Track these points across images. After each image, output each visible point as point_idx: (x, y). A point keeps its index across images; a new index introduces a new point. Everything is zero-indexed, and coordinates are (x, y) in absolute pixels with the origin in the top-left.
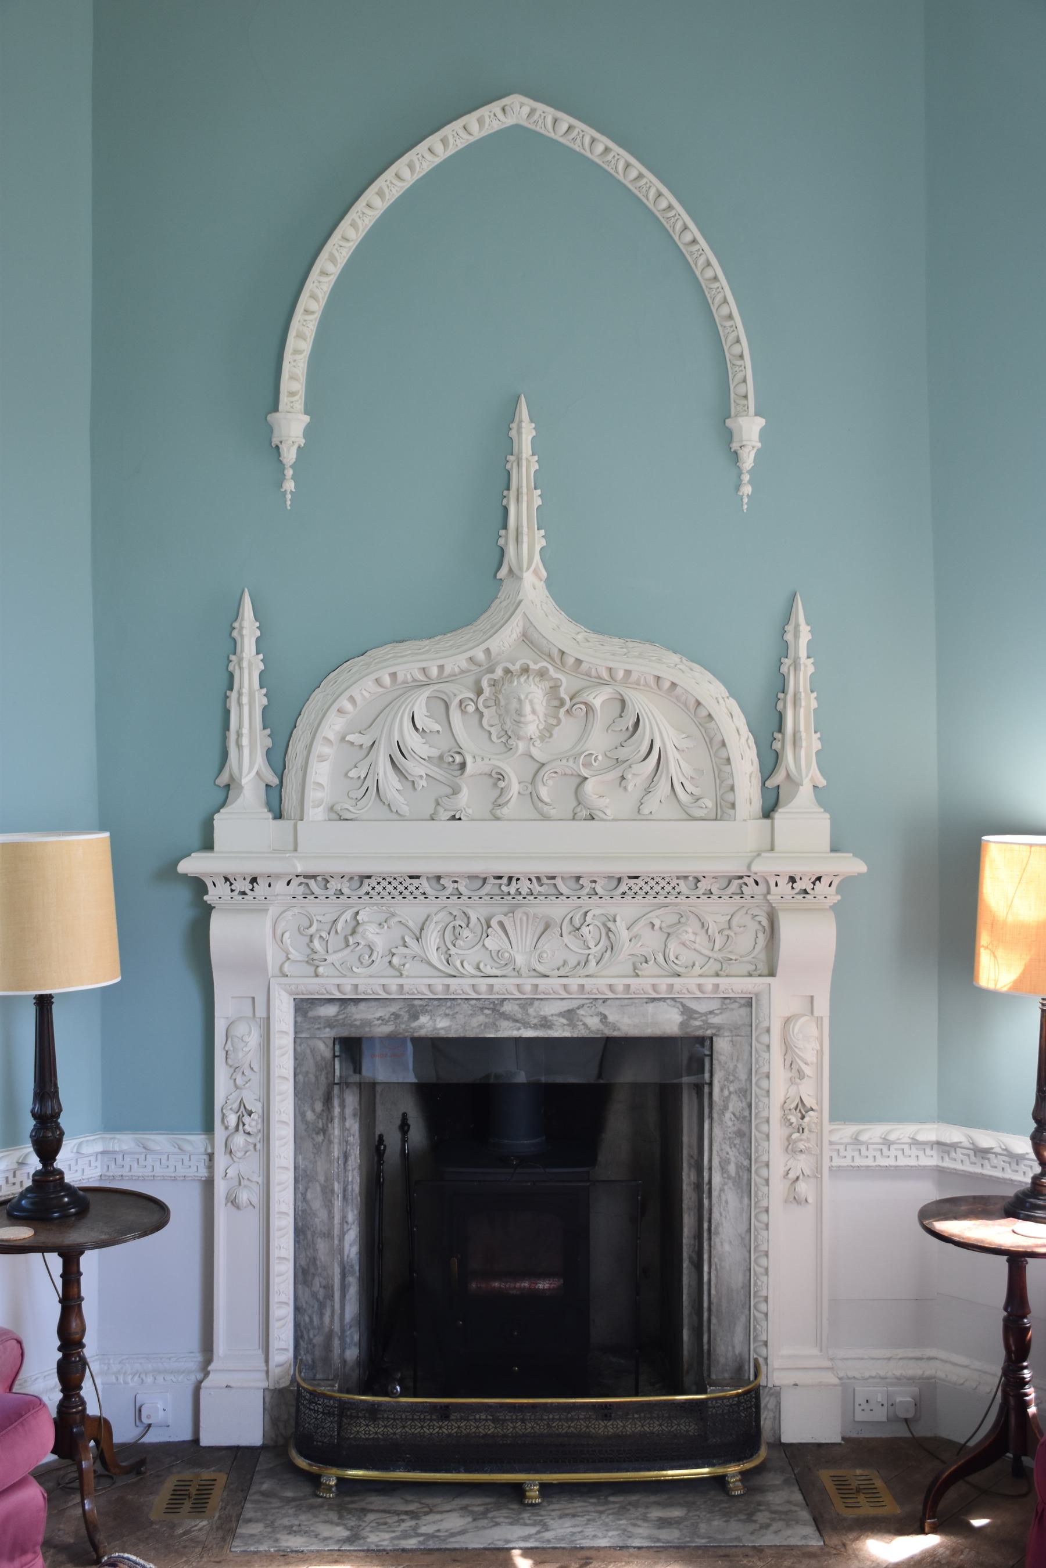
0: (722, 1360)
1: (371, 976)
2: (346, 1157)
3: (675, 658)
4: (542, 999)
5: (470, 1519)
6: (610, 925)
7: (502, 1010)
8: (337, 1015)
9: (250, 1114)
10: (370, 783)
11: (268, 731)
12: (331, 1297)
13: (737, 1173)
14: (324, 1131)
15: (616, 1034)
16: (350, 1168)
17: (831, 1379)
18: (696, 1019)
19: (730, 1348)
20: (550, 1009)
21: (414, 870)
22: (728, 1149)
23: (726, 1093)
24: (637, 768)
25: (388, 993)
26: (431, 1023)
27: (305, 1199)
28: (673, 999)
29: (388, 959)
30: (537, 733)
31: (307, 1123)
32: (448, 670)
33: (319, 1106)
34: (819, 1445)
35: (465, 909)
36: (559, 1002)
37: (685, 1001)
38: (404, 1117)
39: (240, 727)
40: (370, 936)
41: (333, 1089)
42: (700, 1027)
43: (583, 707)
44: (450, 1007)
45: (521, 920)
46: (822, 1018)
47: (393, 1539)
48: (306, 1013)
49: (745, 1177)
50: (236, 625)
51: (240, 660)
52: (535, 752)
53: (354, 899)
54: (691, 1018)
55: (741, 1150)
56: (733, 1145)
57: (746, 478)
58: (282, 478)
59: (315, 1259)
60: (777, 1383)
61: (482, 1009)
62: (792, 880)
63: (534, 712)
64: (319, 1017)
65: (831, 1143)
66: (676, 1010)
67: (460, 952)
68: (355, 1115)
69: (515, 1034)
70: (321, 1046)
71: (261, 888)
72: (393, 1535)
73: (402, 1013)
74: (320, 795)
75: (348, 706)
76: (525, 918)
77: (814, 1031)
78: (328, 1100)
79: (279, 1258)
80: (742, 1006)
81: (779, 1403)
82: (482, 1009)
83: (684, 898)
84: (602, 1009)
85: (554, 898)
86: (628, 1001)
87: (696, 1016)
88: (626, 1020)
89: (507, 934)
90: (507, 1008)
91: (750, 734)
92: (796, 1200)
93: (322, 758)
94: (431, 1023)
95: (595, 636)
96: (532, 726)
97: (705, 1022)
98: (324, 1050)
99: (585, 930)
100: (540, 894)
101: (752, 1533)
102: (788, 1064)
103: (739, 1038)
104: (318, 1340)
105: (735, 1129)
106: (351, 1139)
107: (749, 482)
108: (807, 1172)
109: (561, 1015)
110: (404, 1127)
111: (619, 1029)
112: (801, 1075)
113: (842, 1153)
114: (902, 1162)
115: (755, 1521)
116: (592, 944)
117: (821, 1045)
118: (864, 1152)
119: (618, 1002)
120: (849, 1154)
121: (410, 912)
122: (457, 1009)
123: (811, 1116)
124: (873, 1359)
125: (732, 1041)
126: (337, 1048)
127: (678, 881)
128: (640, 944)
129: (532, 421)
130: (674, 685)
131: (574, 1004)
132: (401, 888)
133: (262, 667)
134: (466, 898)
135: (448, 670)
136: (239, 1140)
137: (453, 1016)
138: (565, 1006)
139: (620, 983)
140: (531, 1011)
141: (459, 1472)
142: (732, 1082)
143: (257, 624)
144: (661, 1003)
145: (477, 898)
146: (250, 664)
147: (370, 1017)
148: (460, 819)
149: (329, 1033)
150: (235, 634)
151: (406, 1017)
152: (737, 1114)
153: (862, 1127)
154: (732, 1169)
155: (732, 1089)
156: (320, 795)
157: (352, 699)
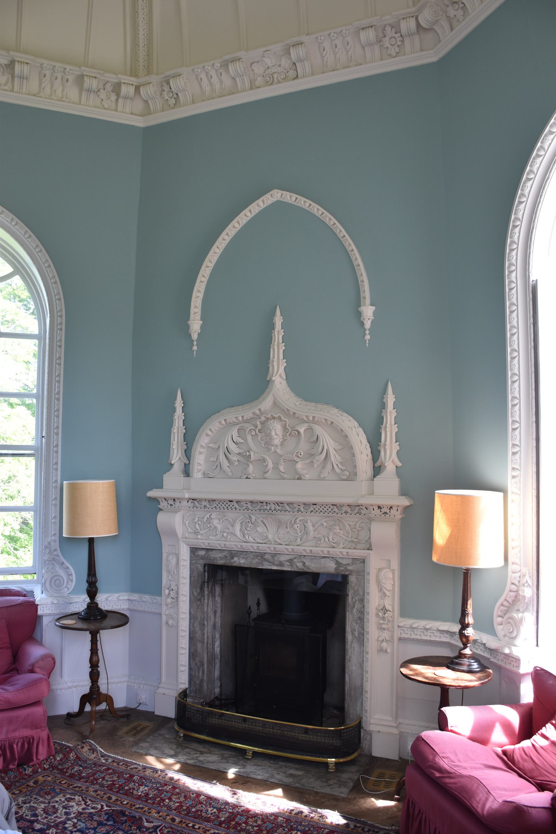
0: (352, 716)
1: (217, 540)
2: (215, 613)
3: (336, 411)
4: (280, 554)
5: (304, 772)
6: (305, 524)
7: (265, 557)
8: (205, 555)
9: (173, 590)
10: (218, 463)
11: (185, 443)
12: (203, 665)
13: (359, 636)
14: (200, 600)
15: (309, 571)
16: (217, 616)
17: (395, 731)
18: (342, 567)
19: (355, 712)
20: (283, 558)
21: (231, 498)
22: (355, 625)
23: (354, 600)
24: (317, 458)
25: (344, 556)
26: (238, 561)
27: (193, 627)
28: (332, 557)
29: (222, 534)
30: (279, 443)
31: (194, 596)
32: (245, 418)
33: (198, 590)
34: (388, 760)
35: (250, 515)
36: (286, 555)
37: (337, 559)
38: (258, 600)
39: (386, 440)
40: (215, 524)
41: (204, 584)
42: (343, 570)
43: (296, 432)
44: (245, 555)
45: (270, 521)
46: (394, 570)
47: (187, 759)
48: (194, 553)
49: (362, 638)
50: (385, 396)
51: (387, 412)
52: (279, 451)
53: (210, 509)
54: (339, 566)
55: (360, 625)
56: (357, 623)
57: (367, 332)
58: (365, 334)
59: (197, 650)
60: (371, 729)
61: (257, 556)
62: (379, 507)
63: (276, 434)
64: (199, 555)
65: (399, 626)
66: (333, 562)
67: (248, 532)
68: (219, 596)
69: (269, 567)
70: (200, 566)
71: (177, 503)
72: (188, 757)
73: (228, 555)
74: (200, 467)
75: (210, 433)
76: (271, 520)
77: (390, 575)
78: (202, 588)
79: (181, 648)
80: (361, 562)
81: (371, 739)
82: (257, 556)
83: (336, 514)
84: (303, 560)
85: (284, 512)
86: (314, 557)
87: (342, 565)
88: (313, 565)
89: (266, 526)
90: (267, 556)
91: (368, 444)
92: (381, 650)
93: (200, 453)
94: (238, 561)
95: (305, 402)
96: (277, 441)
97: (346, 568)
98: (201, 568)
99: (296, 526)
100: (279, 510)
101: (321, 787)
102: (379, 590)
103: (359, 576)
104: (198, 682)
105: (358, 616)
106: (218, 605)
107: (369, 334)
108: (387, 638)
109: (287, 561)
110: (258, 604)
111: (310, 569)
112: (385, 595)
113: (406, 632)
114: (433, 638)
115: (328, 782)
116: (299, 532)
117: (394, 582)
118: (416, 632)
119: (310, 557)
120: (409, 632)
121: (231, 515)
122: (248, 556)
123: (388, 614)
124: (419, 726)
125: (357, 577)
126: (206, 568)
127: (333, 507)
128: (317, 533)
129: (281, 315)
130: (332, 422)
131: (292, 557)
132: (227, 505)
133: (184, 418)
134: (263, 511)
135: (245, 418)
136: (169, 600)
137: (246, 559)
138: (288, 557)
139: (308, 549)
140: (276, 558)
141: (225, 740)
142: (357, 595)
143: (183, 402)
144: (327, 559)
145: (340, 514)
146: (391, 412)
147: (216, 556)
148: (250, 478)
149: (202, 562)
150: (385, 400)
151: (229, 558)
152: (359, 610)
153: (109, 595)
154: (356, 633)
155: (356, 598)
156: (200, 467)
157: (210, 430)
